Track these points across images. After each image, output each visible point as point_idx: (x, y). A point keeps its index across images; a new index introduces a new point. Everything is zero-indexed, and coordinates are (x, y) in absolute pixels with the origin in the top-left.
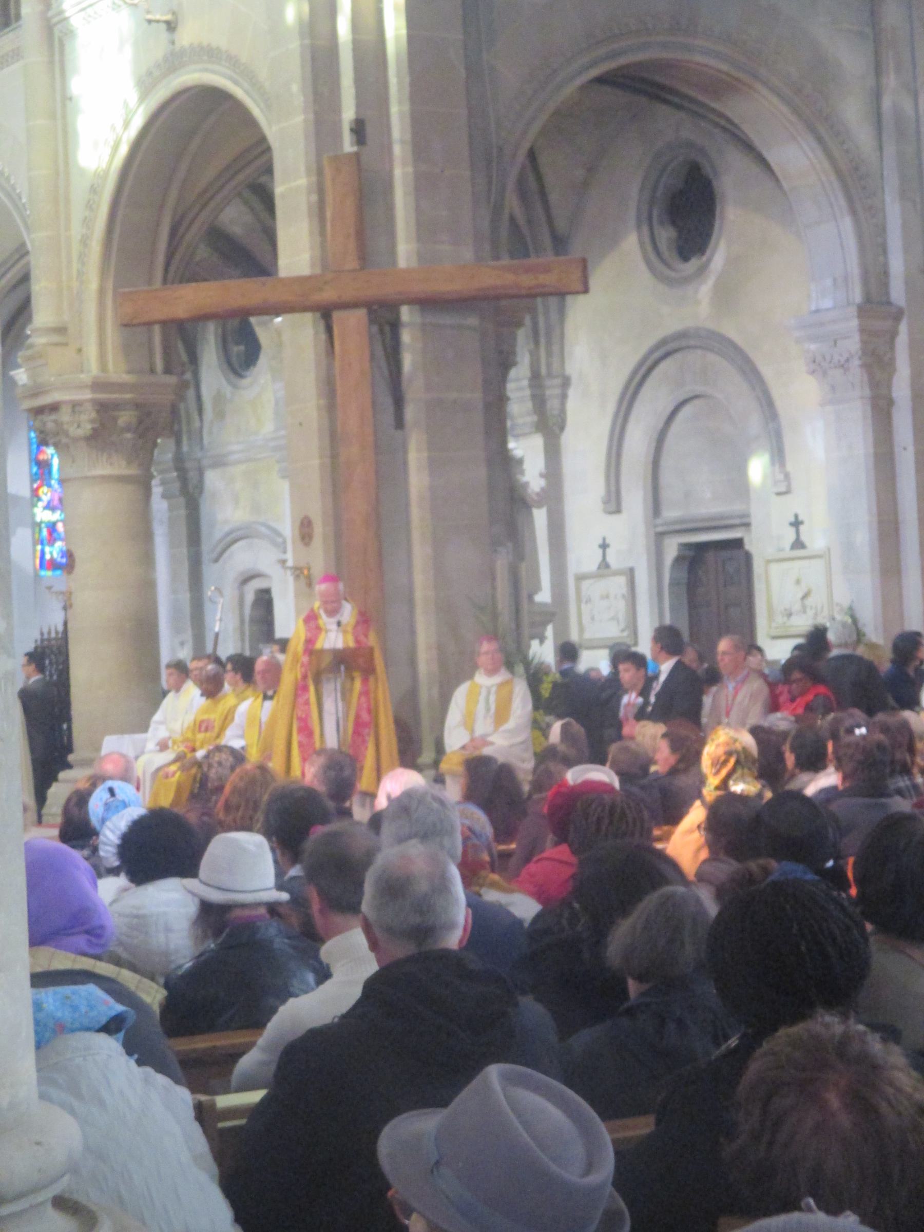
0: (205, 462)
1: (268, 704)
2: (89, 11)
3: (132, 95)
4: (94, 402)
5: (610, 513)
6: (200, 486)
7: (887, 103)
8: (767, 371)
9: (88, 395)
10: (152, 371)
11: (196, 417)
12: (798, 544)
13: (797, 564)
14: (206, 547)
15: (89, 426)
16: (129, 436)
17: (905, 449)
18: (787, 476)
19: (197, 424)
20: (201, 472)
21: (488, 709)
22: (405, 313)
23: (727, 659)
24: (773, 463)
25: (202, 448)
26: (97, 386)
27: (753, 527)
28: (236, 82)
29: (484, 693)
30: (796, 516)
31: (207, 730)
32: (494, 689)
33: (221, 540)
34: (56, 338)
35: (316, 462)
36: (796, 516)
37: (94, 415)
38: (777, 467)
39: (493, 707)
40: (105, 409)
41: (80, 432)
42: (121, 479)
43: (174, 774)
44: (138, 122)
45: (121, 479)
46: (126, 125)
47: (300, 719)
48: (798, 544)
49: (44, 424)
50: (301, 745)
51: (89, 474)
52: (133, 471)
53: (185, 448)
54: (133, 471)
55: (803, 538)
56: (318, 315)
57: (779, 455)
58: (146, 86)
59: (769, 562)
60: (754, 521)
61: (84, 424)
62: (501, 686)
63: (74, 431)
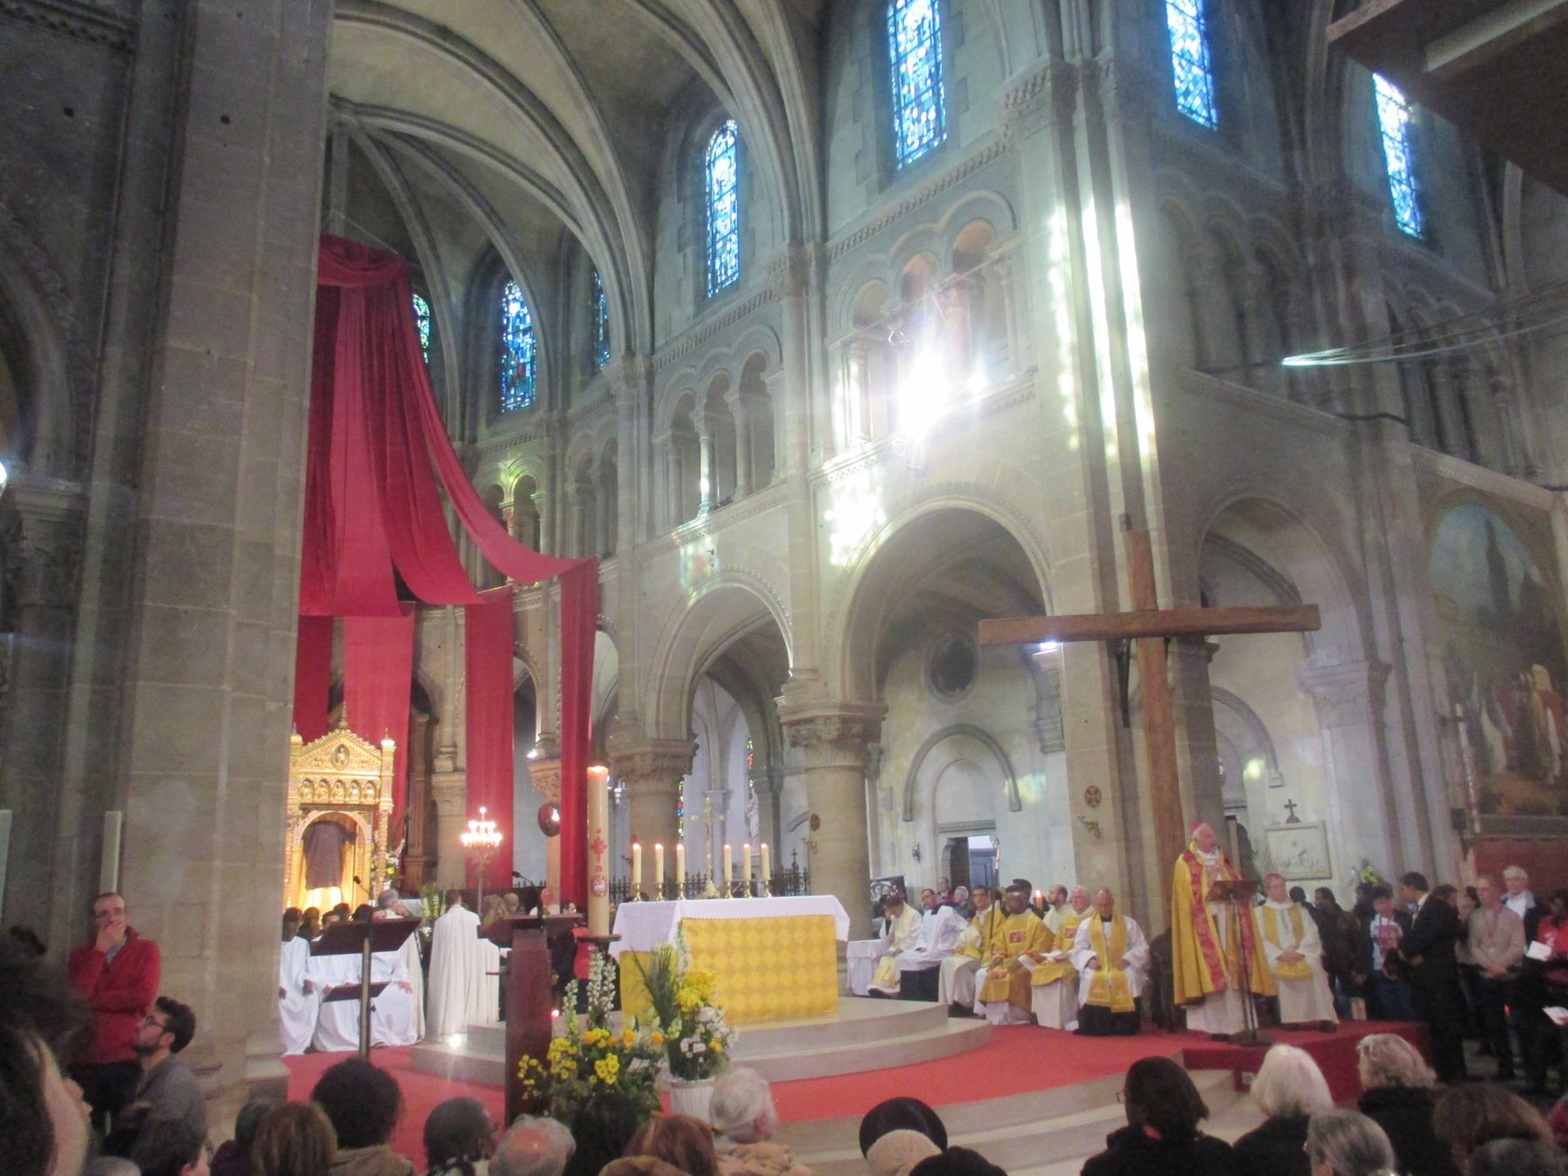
0: (785, 772)
1: (1107, 924)
2: (845, 470)
3: (882, 518)
4: (839, 716)
5: (1014, 811)
6: (781, 786)
7: (1368, 537)
8: (1258, 710)
9: (837, 712)
10: (871, 699)
11: (779, 744)
12: (1293, 819)
13: (1293, 832)
14: (783, 824)
15: (835, 733)
16: (858, 740)
17: (1399, 755)
18: (1281, 775)
19: (780, 748)
20: (782, 778)
21: (1287, 927)
22: (1134, 647)
23: (1486, 894)
24: (1268, 766)
25: (783, 764)
26: (843, 706)
27: (1250, 810)
28: (982, 504)
29: (1278, 917)
30: (1290, 801)
31: (1019, 940)
32: (1286, 912)
33: (794, 821)
34: (811, 676)
35: (1105, 747)
36: (1290, 801)
37: (839, 726)
38: (1273, 771)
39: (1290, 926)
40: (845, 721)
41: (830, 737)
42: (852, 769)
43: (1004, 976)
44: (884, 536)
45: (852, 769)
46: (875, 537)
47: (1201, 935)
48: (1293, 819)
49: (799, 731)
50: (1206, 956)
51: (833, 764)
52: (858, 764)
53: (772, 763)
54: (858, 764)
55: (1296, 815)
56: (1104, 643)
57: (1273, 762)
58: (892, 512)
59: (1268, 831)
60: (1249, 805)
61: (832, 731)
62: (1289, 909)
63: (824, 736)
